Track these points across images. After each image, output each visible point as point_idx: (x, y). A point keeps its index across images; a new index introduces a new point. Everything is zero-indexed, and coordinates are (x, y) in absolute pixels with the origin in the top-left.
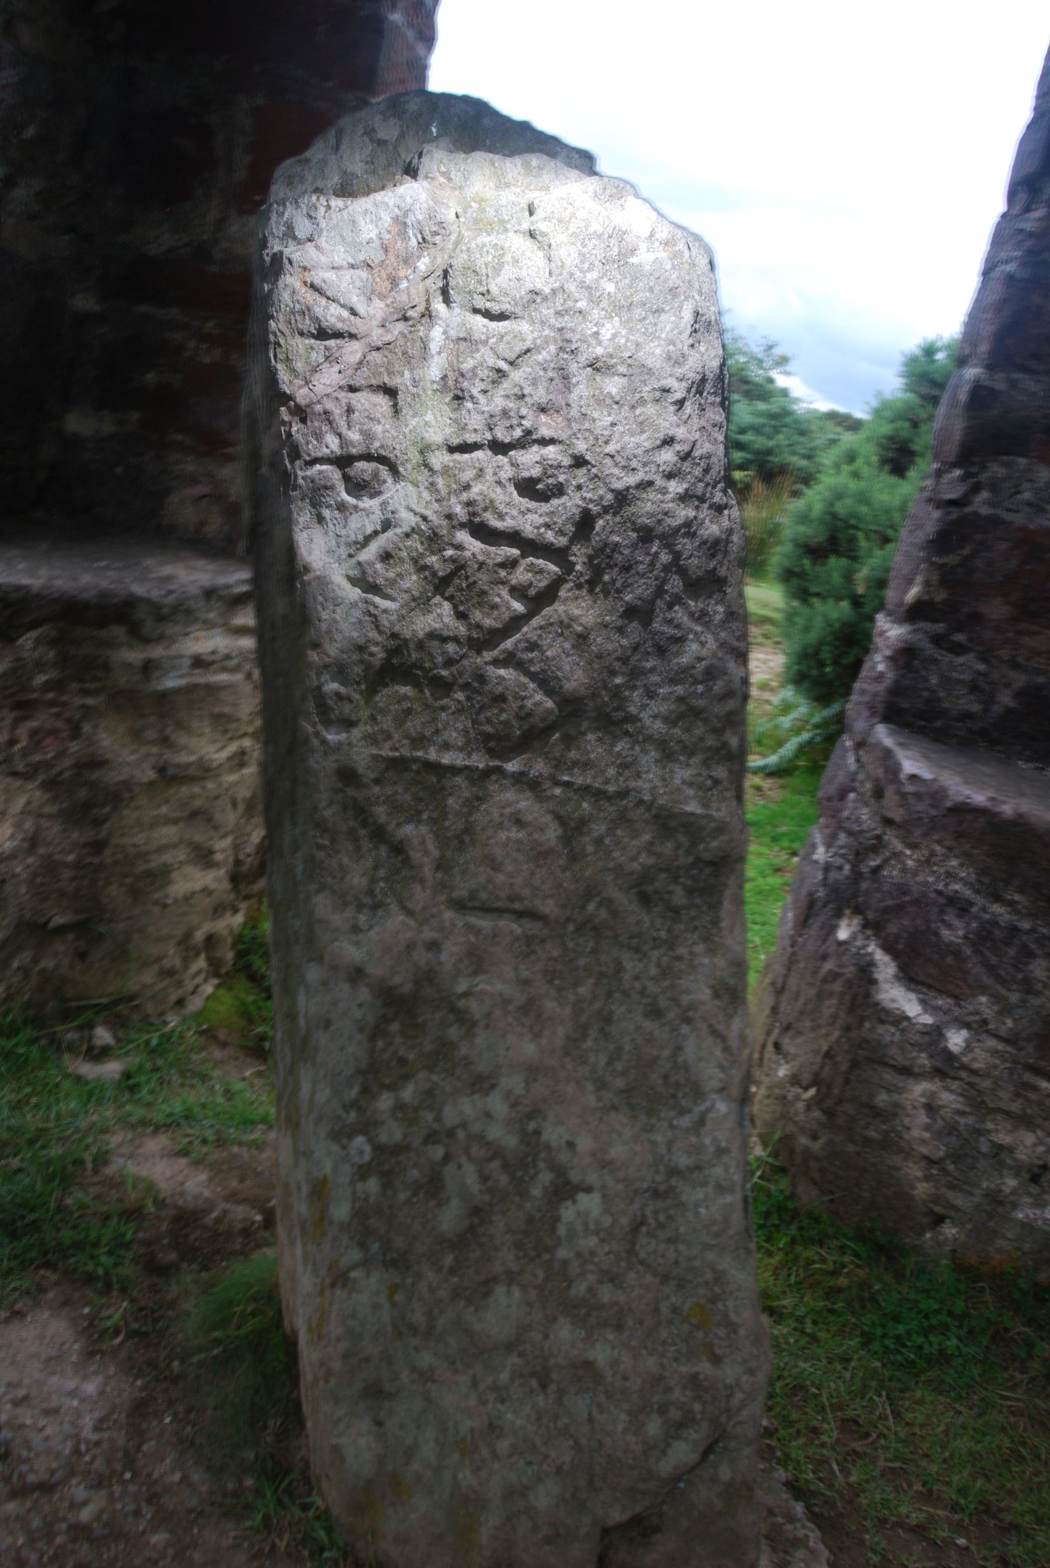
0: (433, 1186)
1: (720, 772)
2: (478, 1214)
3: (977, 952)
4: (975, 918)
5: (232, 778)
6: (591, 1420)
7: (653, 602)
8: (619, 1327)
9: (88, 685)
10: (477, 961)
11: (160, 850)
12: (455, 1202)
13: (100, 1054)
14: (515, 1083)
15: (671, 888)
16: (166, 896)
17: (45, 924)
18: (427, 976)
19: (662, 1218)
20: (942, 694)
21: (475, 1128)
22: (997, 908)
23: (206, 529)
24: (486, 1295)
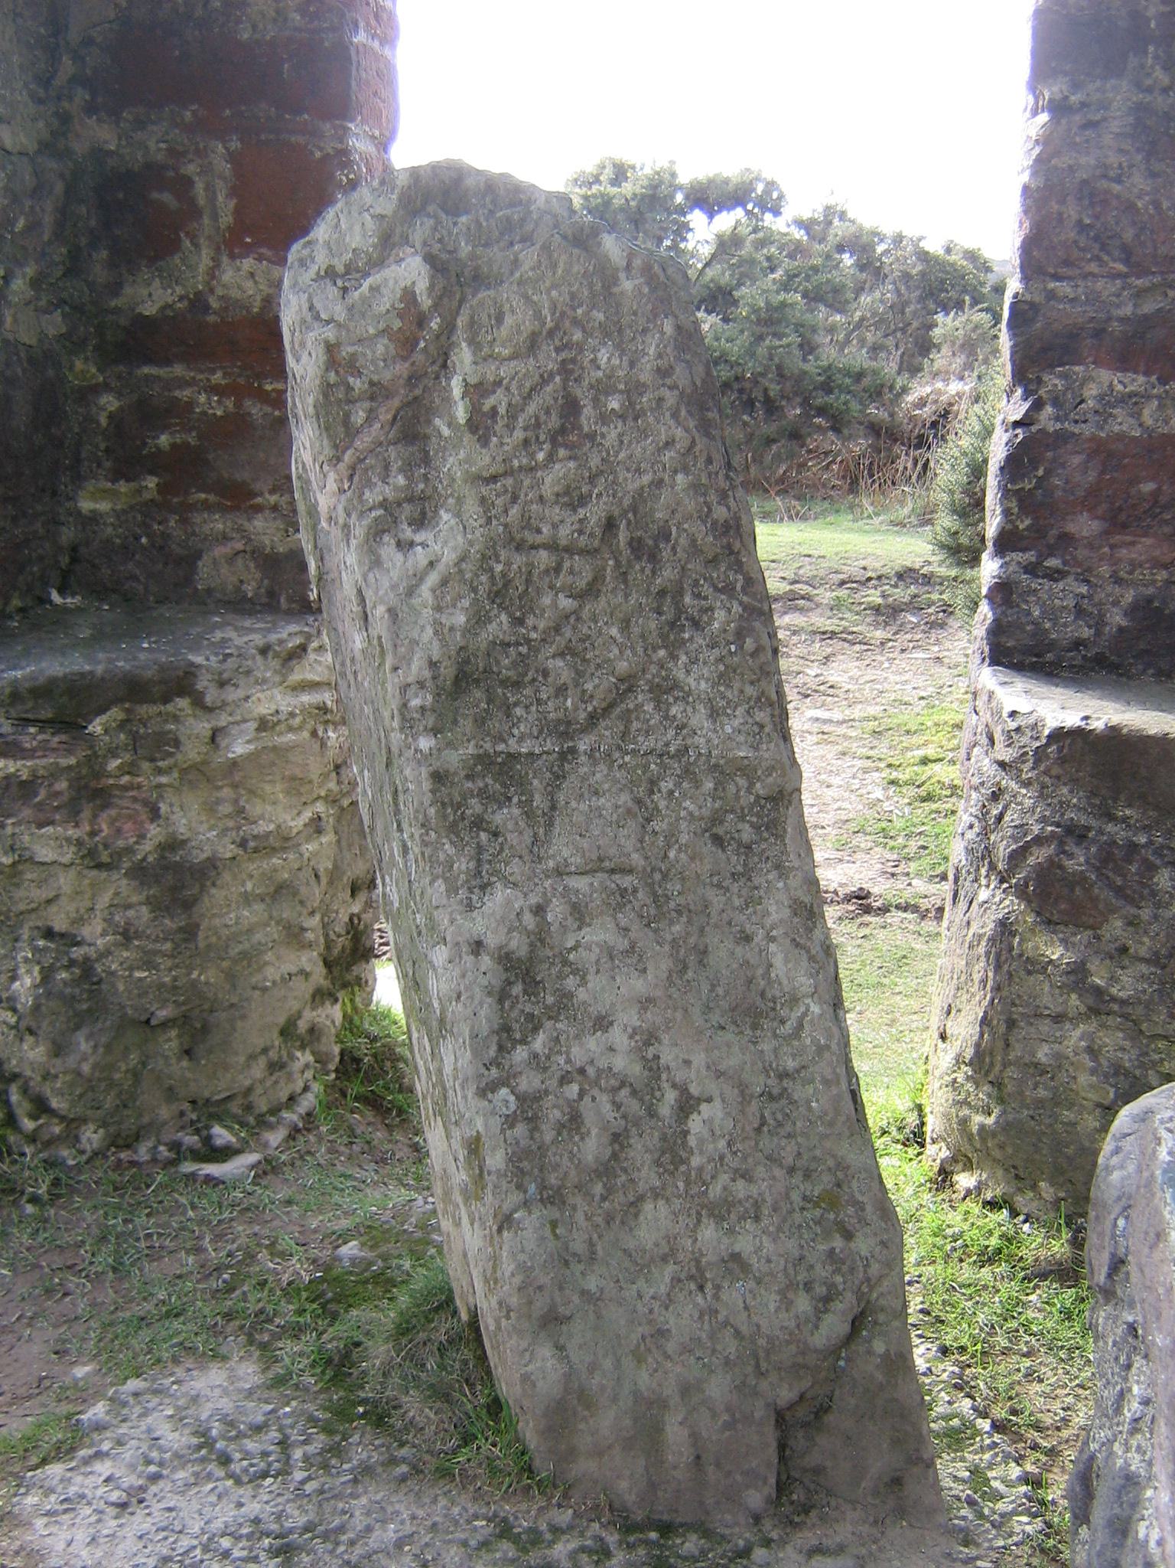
0: (574, 1122)
1: (761, 716)
2: (618, 1139)
3: (1100, 875)
4: (1094, 841)
5: (310, 847)
6: (746, 1308)
7: (680, 582)
8: (757, 1219)
9: (160, 764)
10: (579, 913)
11: (250, 931)
12: (594, 1132)
13: (223, 1154)
14: (630, 1017)
15: (740, 826)
16: (265, 979)
17: (148, 1022)
18: (540, 937)
19: (780, 1117)
20: (1048, 625)
21: (602, 1063)
22: (1110, 828)
23: (245, 587)
24: (636, 1216)
